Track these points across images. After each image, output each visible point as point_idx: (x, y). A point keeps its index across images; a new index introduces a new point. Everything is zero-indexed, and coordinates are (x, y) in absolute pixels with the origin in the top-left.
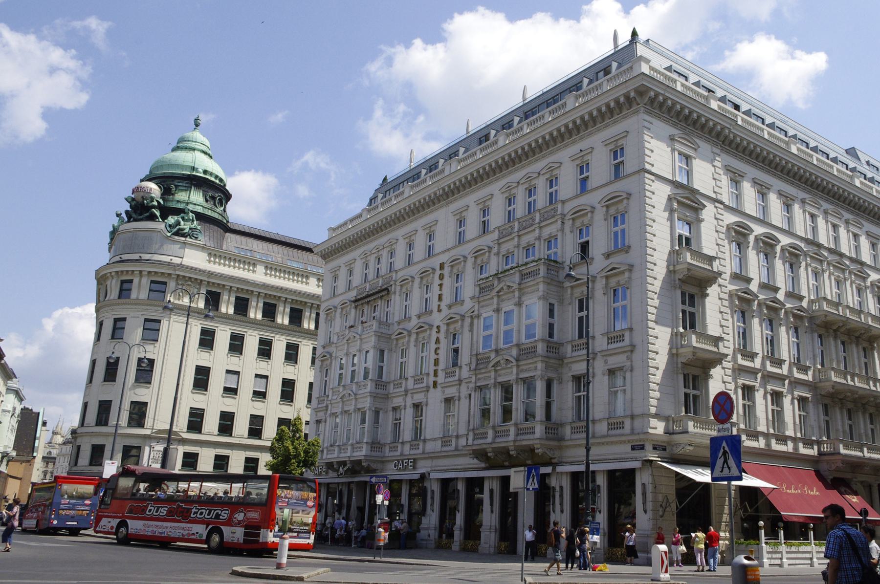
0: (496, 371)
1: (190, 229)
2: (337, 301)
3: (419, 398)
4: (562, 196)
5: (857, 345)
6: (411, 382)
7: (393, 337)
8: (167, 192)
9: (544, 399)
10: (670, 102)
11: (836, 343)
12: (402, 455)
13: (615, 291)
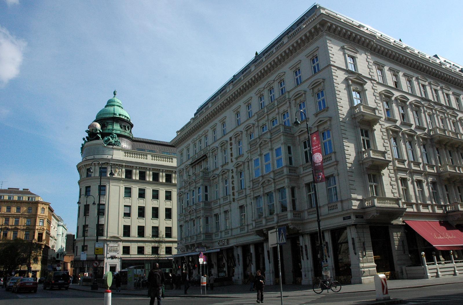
0: (263, 187)
1: (115, 141)
2: (183, 166)
3: (226, 208)
4: (288, 89)
5: (457, 152)
6: (222, 200)
7: (211, 179)
8: (103, 126)
9: (291, 198)
10: (339, 28)
11: (446, 152)
12: (221, 238)
13: (323, 133)
